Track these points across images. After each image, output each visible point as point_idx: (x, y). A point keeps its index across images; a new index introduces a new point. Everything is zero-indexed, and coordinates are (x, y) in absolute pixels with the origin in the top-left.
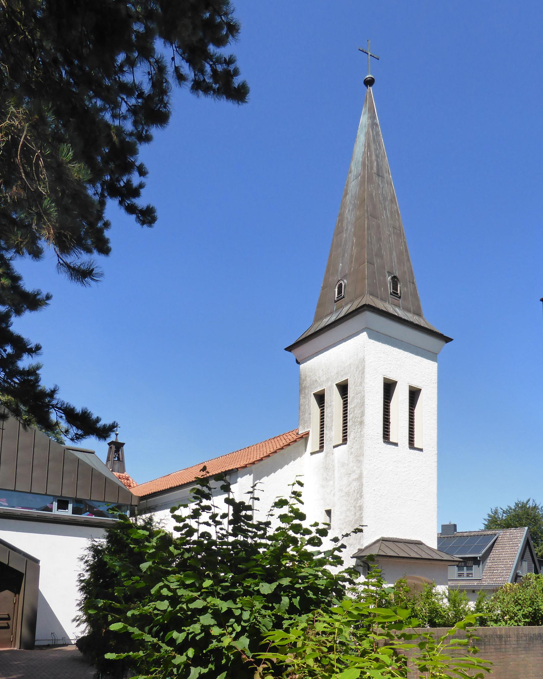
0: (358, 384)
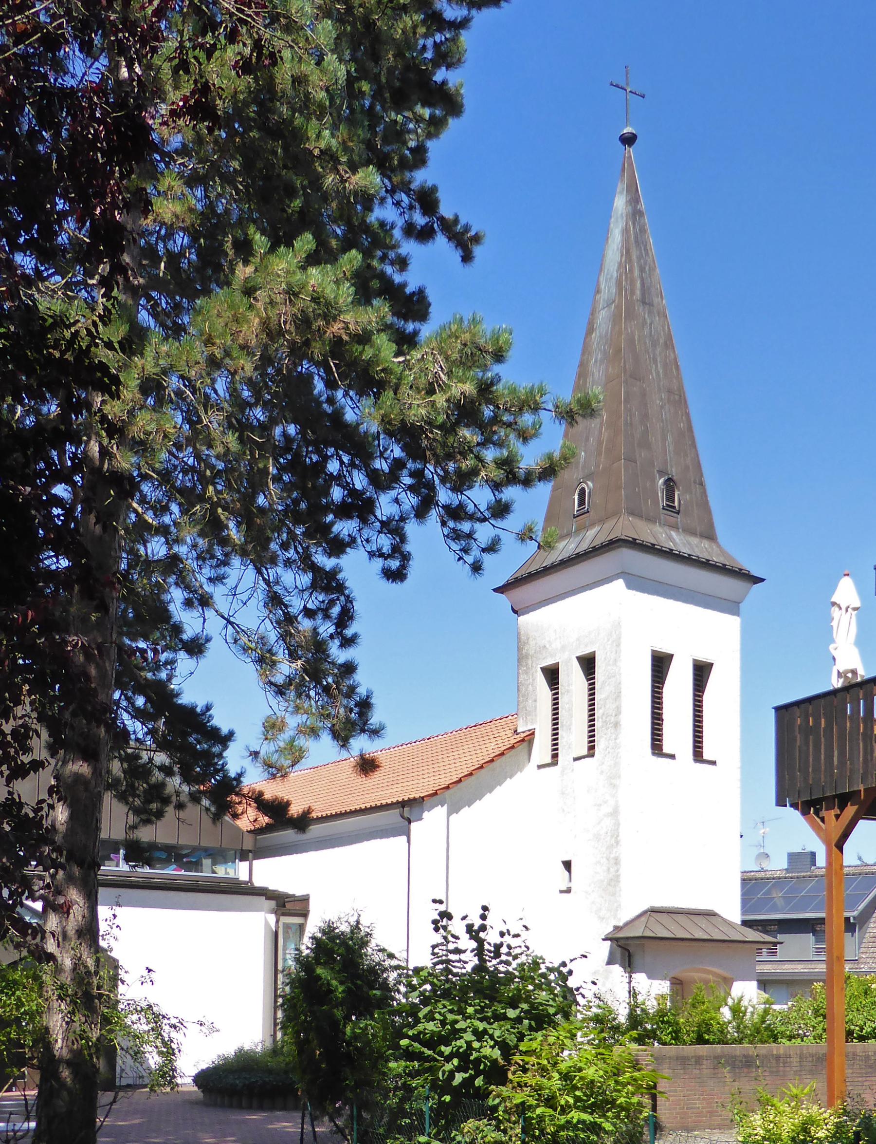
0: (611, 662)
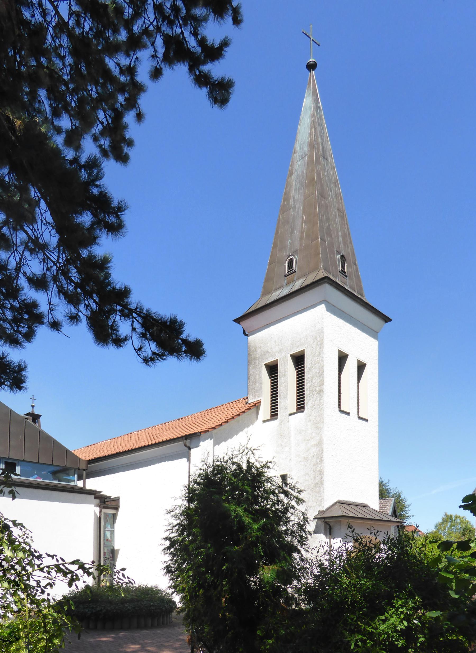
0: (316, 355)
